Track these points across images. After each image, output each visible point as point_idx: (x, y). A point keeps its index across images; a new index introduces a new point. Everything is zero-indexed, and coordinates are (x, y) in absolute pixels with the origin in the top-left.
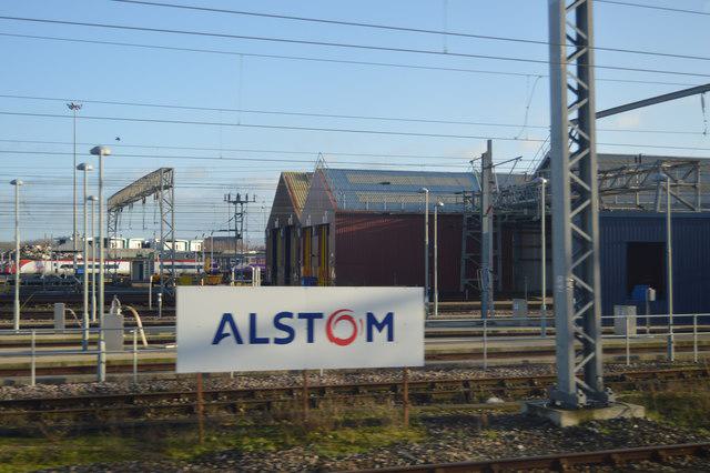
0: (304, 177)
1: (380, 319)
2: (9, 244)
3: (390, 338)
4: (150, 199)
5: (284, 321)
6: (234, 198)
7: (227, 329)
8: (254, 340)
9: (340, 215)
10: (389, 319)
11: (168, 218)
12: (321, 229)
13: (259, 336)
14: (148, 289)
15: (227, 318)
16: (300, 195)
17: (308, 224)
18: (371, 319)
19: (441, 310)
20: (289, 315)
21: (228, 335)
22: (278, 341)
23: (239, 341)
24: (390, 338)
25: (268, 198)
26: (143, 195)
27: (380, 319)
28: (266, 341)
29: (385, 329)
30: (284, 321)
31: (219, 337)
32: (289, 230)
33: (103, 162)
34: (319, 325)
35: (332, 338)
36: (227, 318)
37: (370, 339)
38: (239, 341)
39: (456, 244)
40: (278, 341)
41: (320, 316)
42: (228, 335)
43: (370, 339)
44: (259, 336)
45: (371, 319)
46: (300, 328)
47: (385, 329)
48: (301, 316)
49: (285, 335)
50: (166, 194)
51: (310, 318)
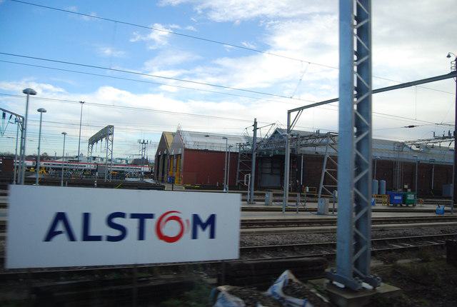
0: (173, 134)
1: (204, 219)
2: (13, 155)
3: (212, 236)
4: (104, 139)
5: (117, 221)
6: (142, 142)
7: (60, 227)
8: (87, 237)
9: (186, 150)
10: (212, 219)
11: (110, 147)
12: (178, 156)
13: (93, 233)
14: (240, 169)
15: (61, 217)
16: (170, 140)
17: (173, 153)
18: (196, 219)
19: (255, 194)
20: (122, 215)
21: (60, 232)
22: (111, 239)
23: (72, 238)
24: (212, 236)
25: (158, 139)
26: (101, 138)
27: (204, 219)
28: (98, 238)
29: (208, 229)
30: (117, 221)
31: (51, 234)
32: (165, 155)
33: (25, 110)
34: (150, 225)
35: (161, 236)
36: (61, 217)
37: (194, 236)
38: (72, 238)
39: (271, 165)
40: (111, 239)
41: (151, 216)
42: (60, 232)
43: (194, 236)
44: (93, 233)
45: (196, 219)
46: (132, 225)
47: (208, 229)
48: (133, 216)
49: (117, 233)
50: (110, 137)
51: (142, 218)
